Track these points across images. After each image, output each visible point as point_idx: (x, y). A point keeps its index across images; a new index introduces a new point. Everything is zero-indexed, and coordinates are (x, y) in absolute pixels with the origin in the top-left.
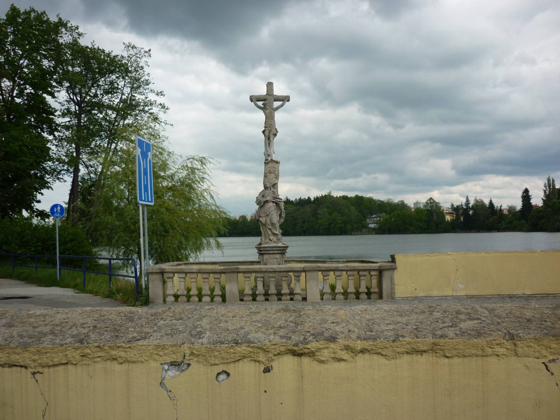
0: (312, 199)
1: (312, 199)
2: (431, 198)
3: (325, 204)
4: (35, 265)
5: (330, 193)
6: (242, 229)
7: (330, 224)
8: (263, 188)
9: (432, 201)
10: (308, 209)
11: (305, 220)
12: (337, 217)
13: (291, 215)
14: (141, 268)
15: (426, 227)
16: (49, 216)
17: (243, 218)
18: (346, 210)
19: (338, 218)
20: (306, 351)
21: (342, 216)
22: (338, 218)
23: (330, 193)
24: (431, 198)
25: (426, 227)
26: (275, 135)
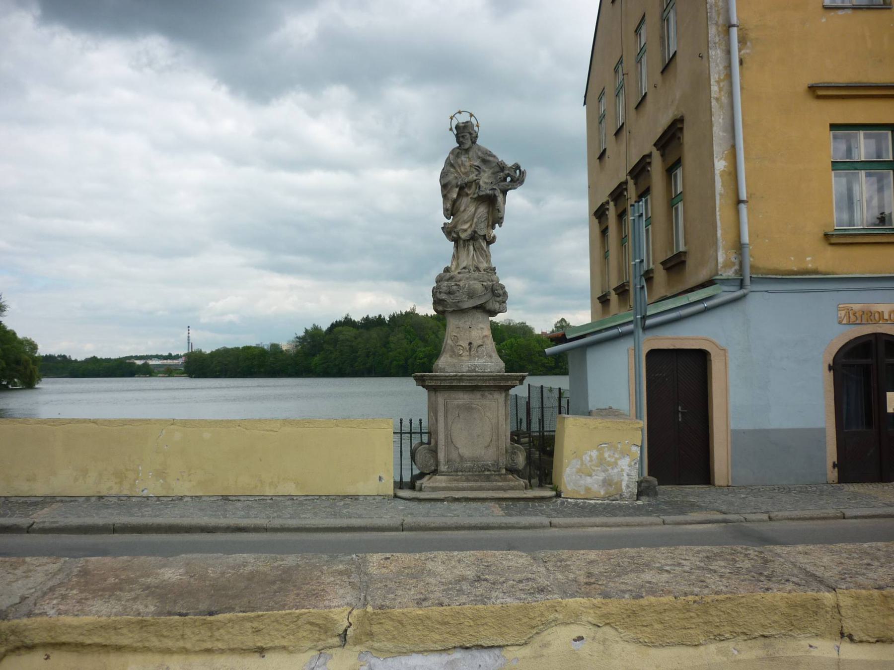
0: (387, 319)
1: (387, 319)
2: (563, 320)
3: (403, 327)
4: (545, 434)
5: (414, 309)
6: (272, 365)
7: (406, 360)
8: (509, 193)
9: (564, 324)
10: (374, 333)
11: (369, 352)
12: (418, 347)
13: (348, 343)
14: (733, 173)
15: (553, 364)
16: (370, 666)
17: (275, 347)
18: (433, 336)
19: (419, 349)
20: (328, 645)
21: (425, 347)
22: (419, 349)
23: (414, 309)
24: (563, 320)
25: (553, 364)
26: (477, 137)
